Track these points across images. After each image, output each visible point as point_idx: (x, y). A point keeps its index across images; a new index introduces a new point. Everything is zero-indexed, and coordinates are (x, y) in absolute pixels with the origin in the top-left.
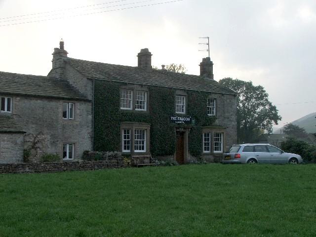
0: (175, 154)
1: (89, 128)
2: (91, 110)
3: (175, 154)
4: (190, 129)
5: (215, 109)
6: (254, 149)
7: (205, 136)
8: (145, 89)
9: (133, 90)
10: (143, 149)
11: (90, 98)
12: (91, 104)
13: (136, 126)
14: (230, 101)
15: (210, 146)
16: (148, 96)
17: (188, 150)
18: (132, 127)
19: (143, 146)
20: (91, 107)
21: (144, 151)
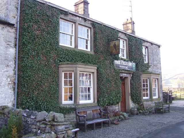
0: (120, 103)
1: (9, 69)
2: (13, 41)
3: (120, 103)
4: (131, 75)
5: (149, 90)
6: (153, 81)
7: (66, 77)
8: (88, 24)
9: (75, 23)
10: (89, 99)
11: (13, 21)
12: (13, 30)
13: (80, 68)
14: (156, 51)
15: (148, 83)
16: (92, 34)
17: (95, 126)
18: (76, 70)
19: (89, 96)
20: (13, 35)
21: (91, 101)
